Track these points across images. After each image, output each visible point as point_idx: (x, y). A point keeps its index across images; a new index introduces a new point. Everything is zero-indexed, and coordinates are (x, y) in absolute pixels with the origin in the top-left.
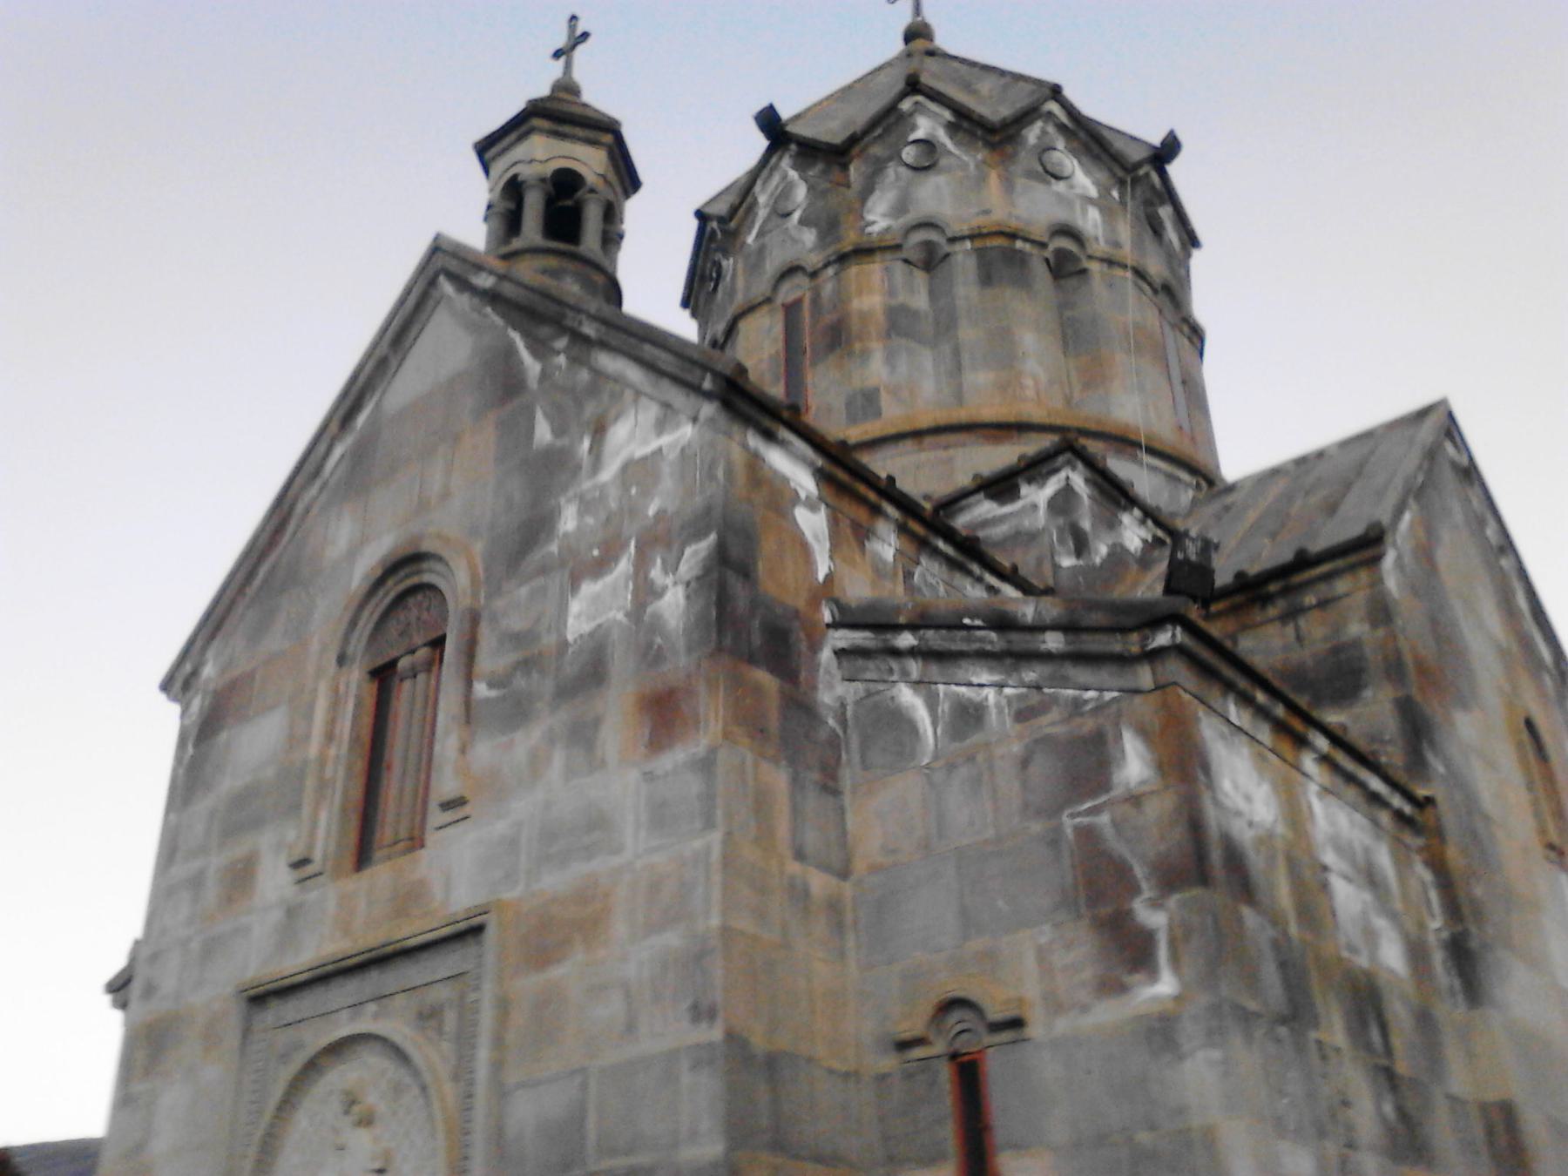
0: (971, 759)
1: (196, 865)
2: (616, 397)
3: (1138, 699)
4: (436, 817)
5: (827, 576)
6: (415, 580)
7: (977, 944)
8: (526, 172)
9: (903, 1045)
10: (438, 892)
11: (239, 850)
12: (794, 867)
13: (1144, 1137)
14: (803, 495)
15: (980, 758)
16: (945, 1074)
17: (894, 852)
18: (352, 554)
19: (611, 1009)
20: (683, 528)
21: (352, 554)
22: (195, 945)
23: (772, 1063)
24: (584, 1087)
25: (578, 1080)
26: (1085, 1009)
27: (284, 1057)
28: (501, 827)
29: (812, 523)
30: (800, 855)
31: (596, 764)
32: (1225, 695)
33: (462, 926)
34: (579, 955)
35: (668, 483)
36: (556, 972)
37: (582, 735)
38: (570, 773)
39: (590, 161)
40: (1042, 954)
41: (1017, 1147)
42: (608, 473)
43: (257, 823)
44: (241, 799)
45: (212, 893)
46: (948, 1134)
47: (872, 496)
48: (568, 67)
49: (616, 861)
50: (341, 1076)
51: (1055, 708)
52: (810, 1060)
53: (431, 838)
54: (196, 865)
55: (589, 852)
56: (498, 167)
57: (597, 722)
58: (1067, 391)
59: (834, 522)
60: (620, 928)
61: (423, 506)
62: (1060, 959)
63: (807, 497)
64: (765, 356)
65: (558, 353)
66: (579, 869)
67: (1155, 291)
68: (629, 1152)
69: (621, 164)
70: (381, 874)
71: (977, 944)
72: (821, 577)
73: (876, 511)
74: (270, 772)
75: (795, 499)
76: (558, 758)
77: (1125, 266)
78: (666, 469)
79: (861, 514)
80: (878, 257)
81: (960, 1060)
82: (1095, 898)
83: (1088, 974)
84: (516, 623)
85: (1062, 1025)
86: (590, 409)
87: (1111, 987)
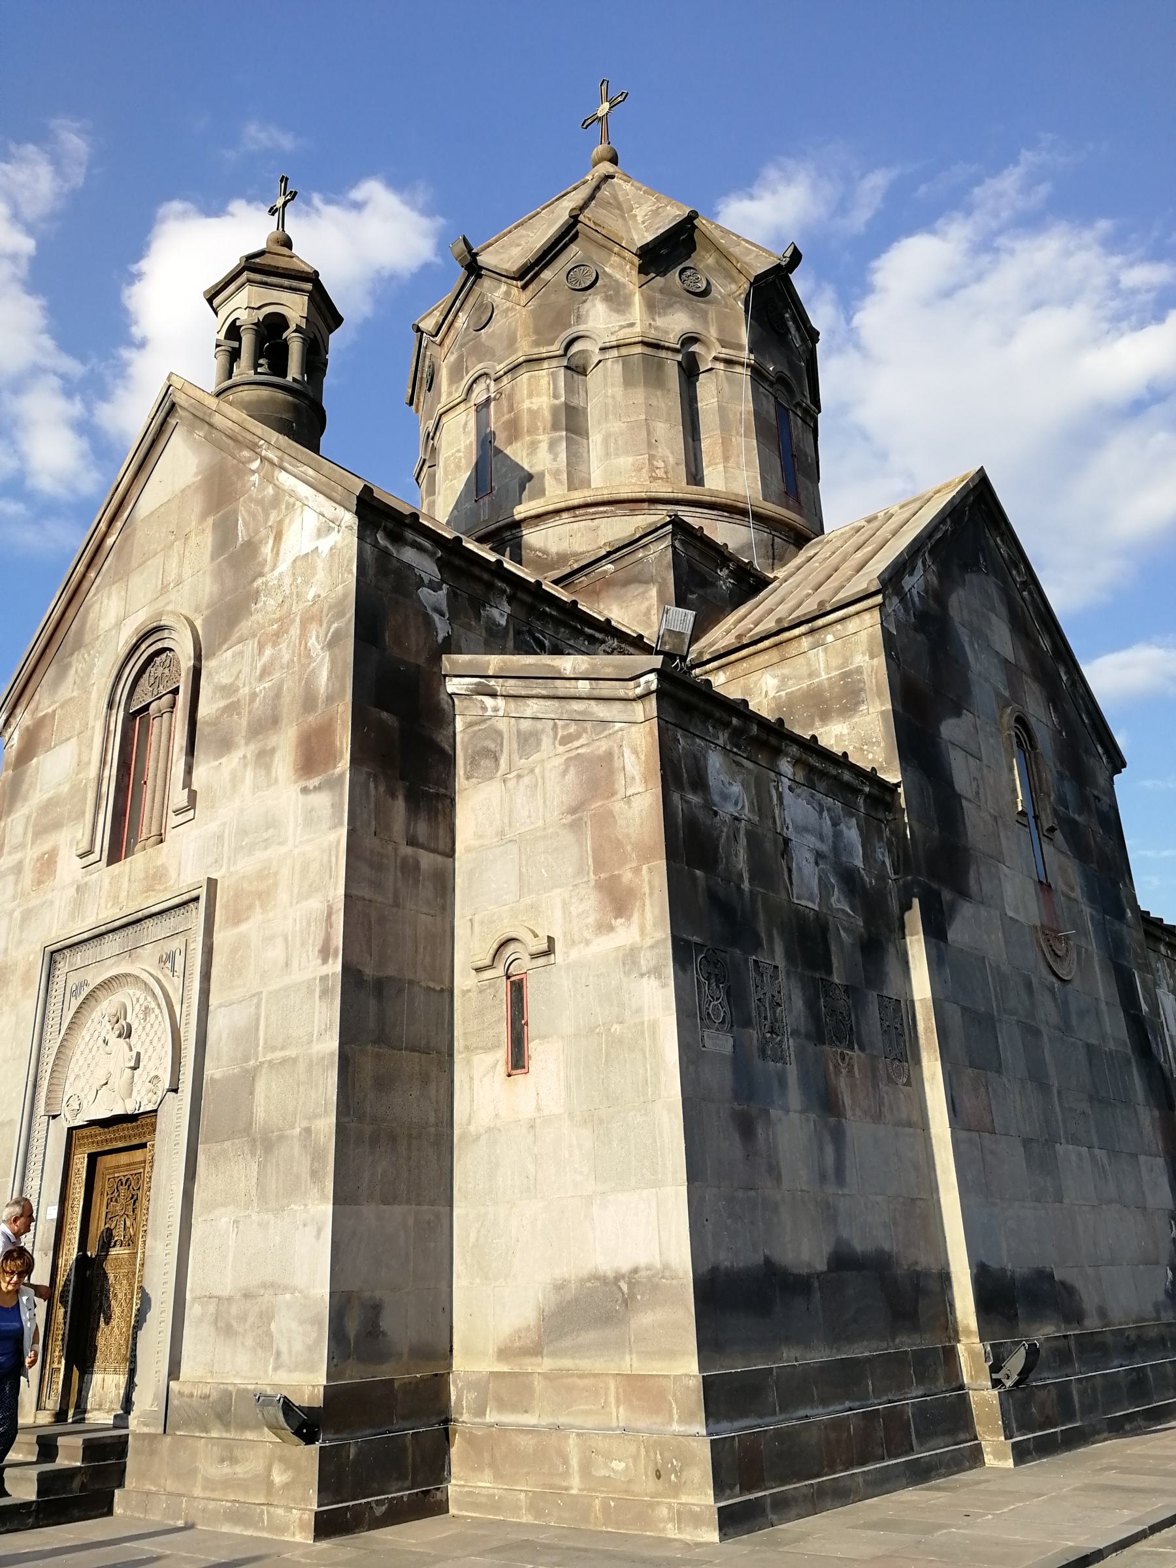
0: (532, 771)
1: (17, 856)
2: (290, 507)
3: (634, 728)
4: (173, 820)
5: (445, 638)
6: (159, 645)
7: (527, 900)
8: (244, 317)
9: (478, 970)
10: (173, 873)
11: (46, 846)
12: (409, 850)
13: (616, 1028)
14: (426, 580)
15: (537, 771)
16: (503, 986)
17: (481, 837)
18: (118, 625)
19: (276, 952)
20: (330, 608)
21: (118, 625)
22: (17, 915)
23: (380, 986)
24: (258, 1006)
25: (255, 1000)
26: (588, 943)
27: (74, 994)
28: (213, 827)
29: (434, 598)
30: (412, 842)
31: (271, 782)
32: (704, 722)
33: (186, 897)
34: (257, 916)
35: (321, 575)
36: (244, 927)
37: (264, 757)
38: (256, 788)
39: (295, 308)
40: (565, 905)
41: (543, 1037)
42: (284, 566)
43: (57, 825)
44: (48, 806)
45: (28, 876)
46: (503, 1031)
47: (486, 576)
48: (282, 223)
49: (283, 850)
50: (107, 1005)
51: (584, 735)
52: (411, 982)
53: (169, 835)
54: (17, 856)
55: (267, 843)
56: (224, 312)
57: (273, 751)
58: (693, 470)
59: (452, 596)
60: (283, 896)
61: (164, 590)
62: (576, 909)
63: (430, 581)
64: (462, 447)
65: (254, 472)
66: (261, 855)
67: (772, 384)
68: (283, 1048)
69: (322, 306)
70: (136, 863)
71: (527, 900)
72: (440, 638)
73: (490, 586)
74: (65, 788)
75: (421, 583)
76: (249, 774)
77: (742, 364)
78: (320, 565)
79: (479, 590)
80: (546, 365)
81: (512, 979)
82: (599, 865)
83: (591, 920)
84: (224, 679)
85: (574, 954)
86: (273, 517)
87: (605, 928)
